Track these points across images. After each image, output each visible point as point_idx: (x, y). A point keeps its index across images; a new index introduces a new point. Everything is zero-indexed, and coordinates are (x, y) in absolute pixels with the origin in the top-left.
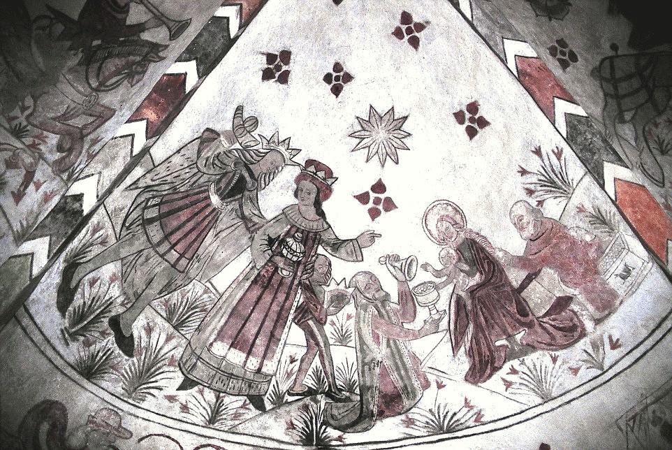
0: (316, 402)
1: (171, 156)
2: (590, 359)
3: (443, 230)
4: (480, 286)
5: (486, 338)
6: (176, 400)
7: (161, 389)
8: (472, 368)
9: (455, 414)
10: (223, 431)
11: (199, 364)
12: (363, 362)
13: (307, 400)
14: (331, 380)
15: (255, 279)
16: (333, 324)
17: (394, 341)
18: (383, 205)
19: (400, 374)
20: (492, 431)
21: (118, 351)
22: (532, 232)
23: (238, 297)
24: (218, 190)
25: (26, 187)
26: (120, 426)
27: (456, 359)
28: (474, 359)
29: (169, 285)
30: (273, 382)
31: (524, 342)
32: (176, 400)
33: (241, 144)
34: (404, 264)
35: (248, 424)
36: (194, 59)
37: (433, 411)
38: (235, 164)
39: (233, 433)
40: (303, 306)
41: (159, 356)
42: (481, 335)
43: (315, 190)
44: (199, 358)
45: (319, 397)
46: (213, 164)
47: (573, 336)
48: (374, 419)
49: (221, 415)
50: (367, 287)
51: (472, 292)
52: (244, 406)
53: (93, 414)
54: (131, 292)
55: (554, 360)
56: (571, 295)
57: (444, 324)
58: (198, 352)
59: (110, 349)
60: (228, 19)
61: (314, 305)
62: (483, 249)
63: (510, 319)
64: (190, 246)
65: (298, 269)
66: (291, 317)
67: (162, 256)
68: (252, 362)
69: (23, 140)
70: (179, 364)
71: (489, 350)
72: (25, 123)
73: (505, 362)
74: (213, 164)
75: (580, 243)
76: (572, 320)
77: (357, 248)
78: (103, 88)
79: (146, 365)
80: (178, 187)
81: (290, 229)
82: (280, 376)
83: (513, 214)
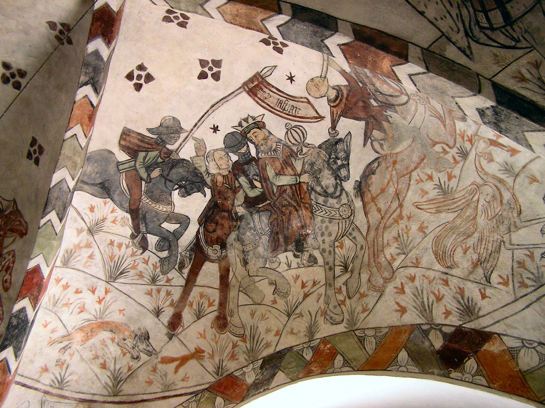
1: (429, 20)
25: (503, 146)
36: (323, 42)
60: (278, 27)
69: (468, 150)
72: (455, 150)
78: (404, 91)
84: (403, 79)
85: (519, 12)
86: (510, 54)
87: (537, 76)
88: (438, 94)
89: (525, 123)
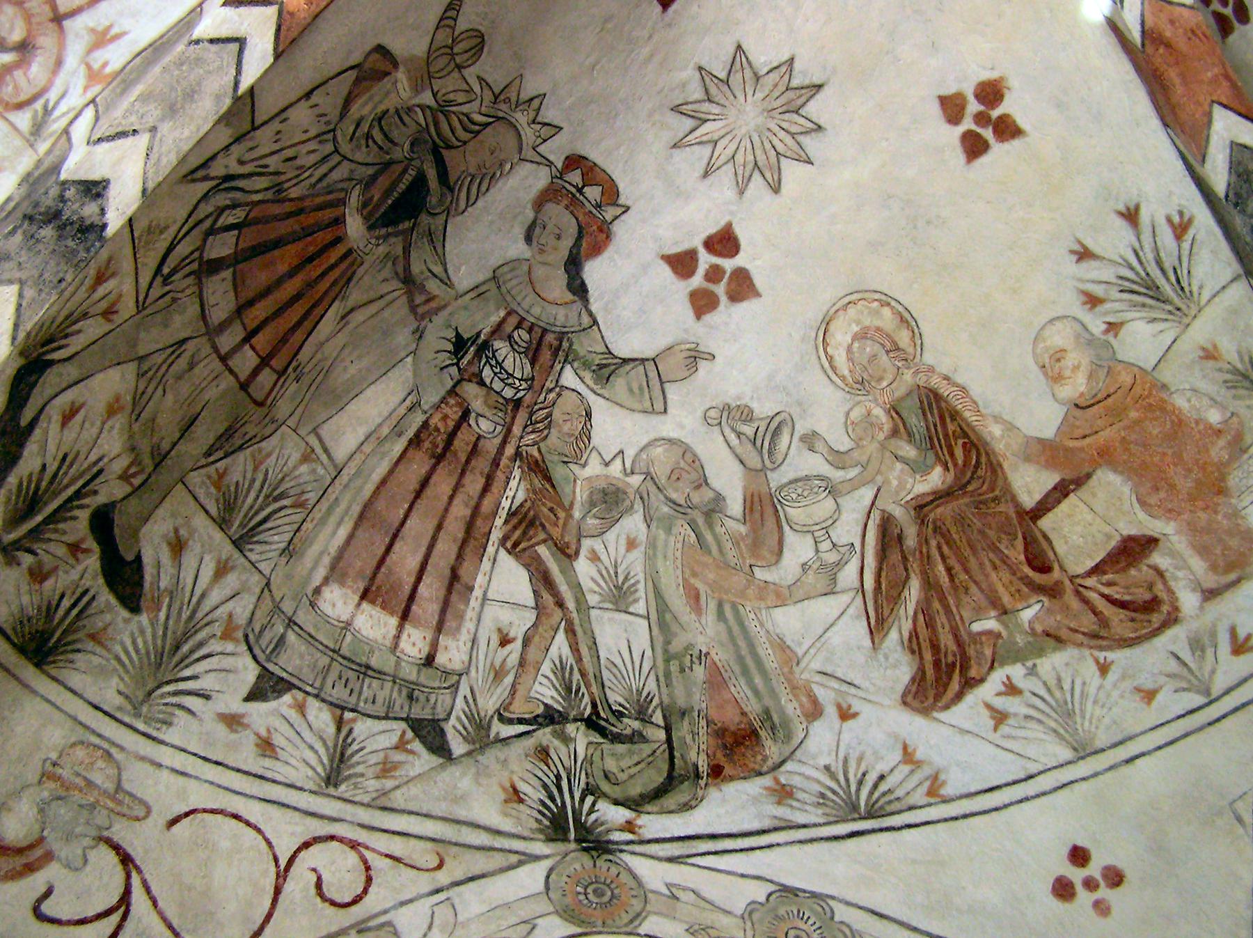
0: (566, 739)
2: (1185, 672)
3: (865, 362)
4: (940, 496)
5: (948, 611)
6: (247, 726)
7: (208, 697)
8: (919, 679)
9: (882, 777)
10: (362, 804)
11: (291, 637)
12: (666, 651)
13: (545, 735)
14: (594, 689)
15: (417, 435)
16: (594, 558)
17: (734, 606)
18: (729, 284)
19: (750, 683)
20: (965, 816)
21: (106, 597)
22: (1082, 389)
23: (377, 476)
24: (365, 205)
26: (119, 787)
27: (881, 657)
28: (921, 658)
29: (228, 434)
30: (464, 690)
31: (1039, 628)
32: (247, 726)
33: (435, 95)
34: (762, 429)
35: (414, 790)
37: (833, 769)
38: (412, 144)
39: (384, 809)
40: (524, 510)
41: (200, 615)
42: (936, 605)
43: (573, 230)
44: (291, 622)
45: (571, 728)
46: (368, 136)
47: (1150, 621)
48: (703, 783)
49: (353, 766)
50: (674, 477)
51: (921, 508)
52: (401, 746)
53: (54, 756)
54: (145, 446)
55: (1104, 669)
56: (1156, 535)
57: (849, 574)
58: (288, 607)
59: (86, 592)
61: (551, 510)
62: (955, 415)
63: (1006, 575)
64: (284, 340)
65: (514, 418)
66: (496, 535)
67: (224, 359)
68: (412, 639)
70: (246, 636)
71: (959, 644)
73: (992, 667)
74: (368, 136)
75: (1193, 425)
76: (1150, 587)
77: (655, 382)
79: (169, 633)
80: (286, 186)
81: (503, 321)
82: (478, 676)
83: (1042, 345)
84: (240, 16)
85: (210, 291)
86: (150, 261)
87: (92, 311)
88: (173, 95)
89: (43, 295)
